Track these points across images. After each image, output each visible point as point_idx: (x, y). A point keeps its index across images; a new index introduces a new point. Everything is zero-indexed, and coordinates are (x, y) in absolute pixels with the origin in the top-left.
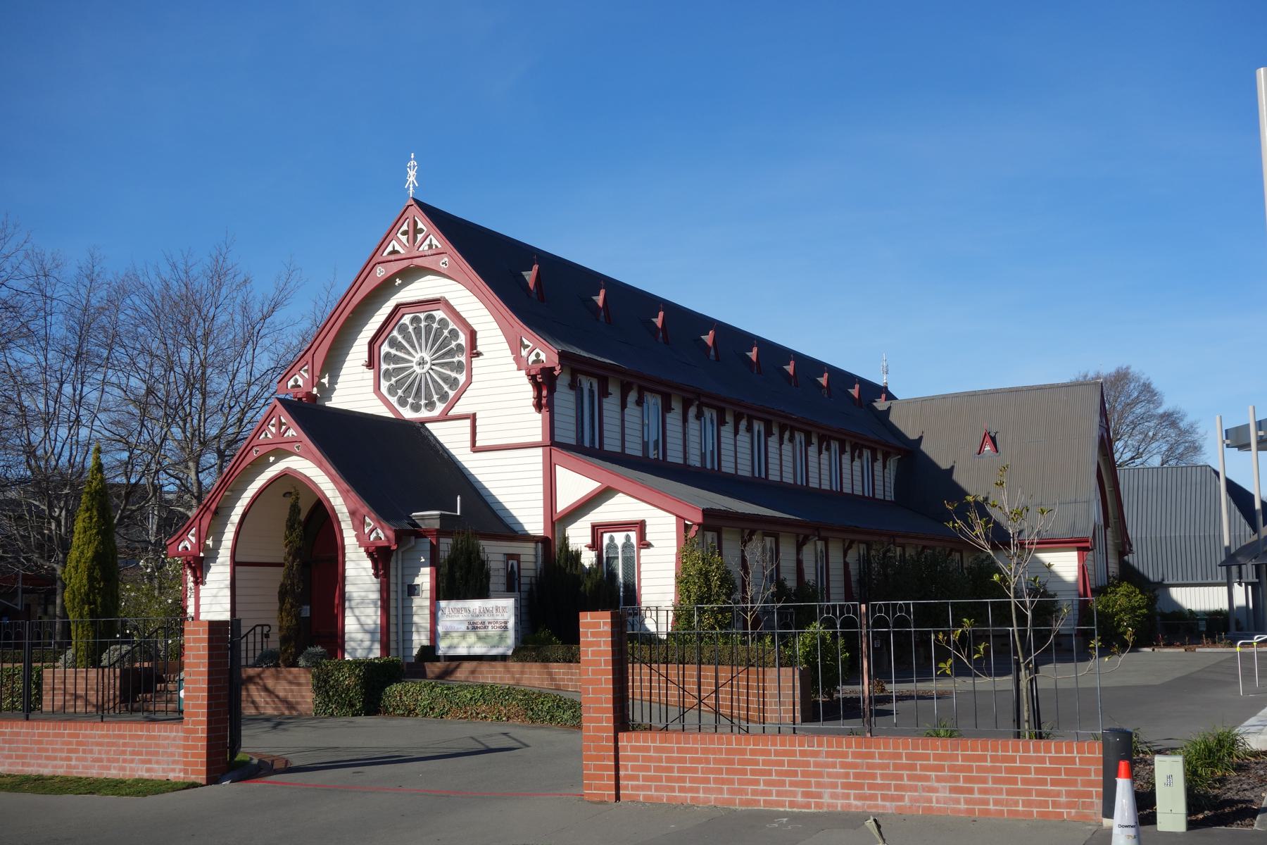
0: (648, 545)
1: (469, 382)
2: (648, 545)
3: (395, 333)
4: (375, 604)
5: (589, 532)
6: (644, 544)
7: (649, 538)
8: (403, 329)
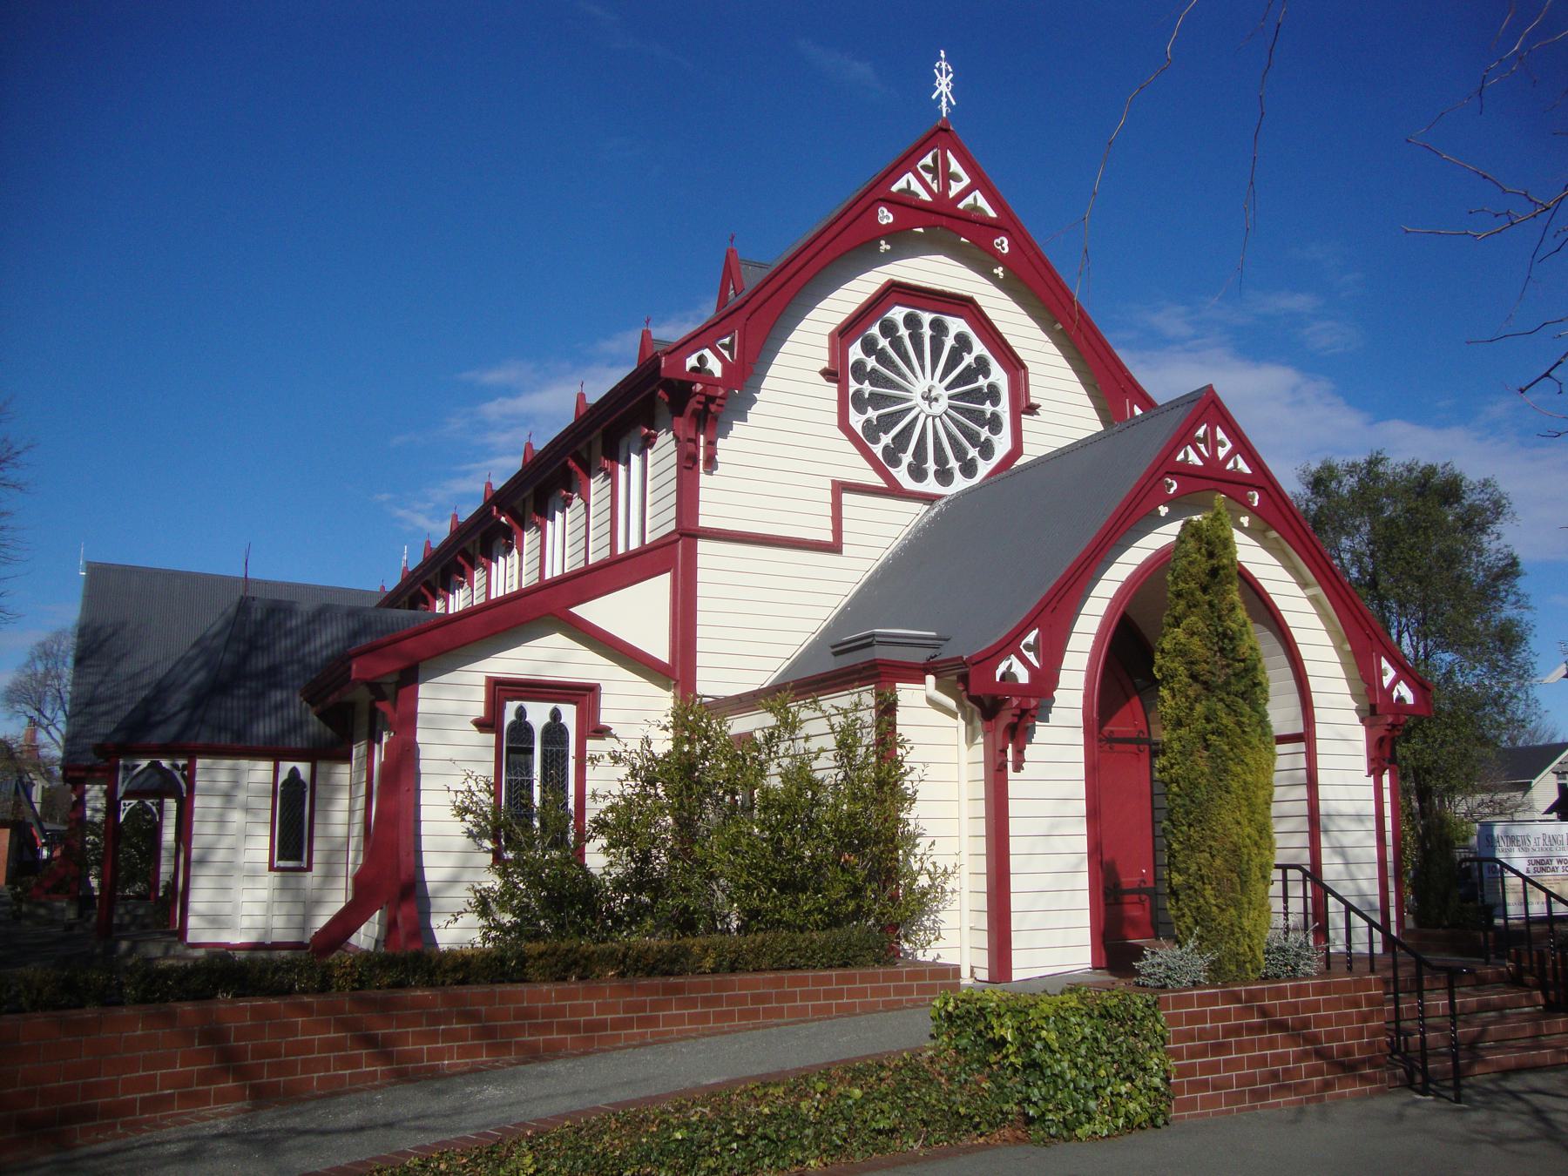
1: (844, 425)
3: (875, 330)
5: (481, 695)
6: (593, 728)
7: (605, 718)
8: (889, 329)
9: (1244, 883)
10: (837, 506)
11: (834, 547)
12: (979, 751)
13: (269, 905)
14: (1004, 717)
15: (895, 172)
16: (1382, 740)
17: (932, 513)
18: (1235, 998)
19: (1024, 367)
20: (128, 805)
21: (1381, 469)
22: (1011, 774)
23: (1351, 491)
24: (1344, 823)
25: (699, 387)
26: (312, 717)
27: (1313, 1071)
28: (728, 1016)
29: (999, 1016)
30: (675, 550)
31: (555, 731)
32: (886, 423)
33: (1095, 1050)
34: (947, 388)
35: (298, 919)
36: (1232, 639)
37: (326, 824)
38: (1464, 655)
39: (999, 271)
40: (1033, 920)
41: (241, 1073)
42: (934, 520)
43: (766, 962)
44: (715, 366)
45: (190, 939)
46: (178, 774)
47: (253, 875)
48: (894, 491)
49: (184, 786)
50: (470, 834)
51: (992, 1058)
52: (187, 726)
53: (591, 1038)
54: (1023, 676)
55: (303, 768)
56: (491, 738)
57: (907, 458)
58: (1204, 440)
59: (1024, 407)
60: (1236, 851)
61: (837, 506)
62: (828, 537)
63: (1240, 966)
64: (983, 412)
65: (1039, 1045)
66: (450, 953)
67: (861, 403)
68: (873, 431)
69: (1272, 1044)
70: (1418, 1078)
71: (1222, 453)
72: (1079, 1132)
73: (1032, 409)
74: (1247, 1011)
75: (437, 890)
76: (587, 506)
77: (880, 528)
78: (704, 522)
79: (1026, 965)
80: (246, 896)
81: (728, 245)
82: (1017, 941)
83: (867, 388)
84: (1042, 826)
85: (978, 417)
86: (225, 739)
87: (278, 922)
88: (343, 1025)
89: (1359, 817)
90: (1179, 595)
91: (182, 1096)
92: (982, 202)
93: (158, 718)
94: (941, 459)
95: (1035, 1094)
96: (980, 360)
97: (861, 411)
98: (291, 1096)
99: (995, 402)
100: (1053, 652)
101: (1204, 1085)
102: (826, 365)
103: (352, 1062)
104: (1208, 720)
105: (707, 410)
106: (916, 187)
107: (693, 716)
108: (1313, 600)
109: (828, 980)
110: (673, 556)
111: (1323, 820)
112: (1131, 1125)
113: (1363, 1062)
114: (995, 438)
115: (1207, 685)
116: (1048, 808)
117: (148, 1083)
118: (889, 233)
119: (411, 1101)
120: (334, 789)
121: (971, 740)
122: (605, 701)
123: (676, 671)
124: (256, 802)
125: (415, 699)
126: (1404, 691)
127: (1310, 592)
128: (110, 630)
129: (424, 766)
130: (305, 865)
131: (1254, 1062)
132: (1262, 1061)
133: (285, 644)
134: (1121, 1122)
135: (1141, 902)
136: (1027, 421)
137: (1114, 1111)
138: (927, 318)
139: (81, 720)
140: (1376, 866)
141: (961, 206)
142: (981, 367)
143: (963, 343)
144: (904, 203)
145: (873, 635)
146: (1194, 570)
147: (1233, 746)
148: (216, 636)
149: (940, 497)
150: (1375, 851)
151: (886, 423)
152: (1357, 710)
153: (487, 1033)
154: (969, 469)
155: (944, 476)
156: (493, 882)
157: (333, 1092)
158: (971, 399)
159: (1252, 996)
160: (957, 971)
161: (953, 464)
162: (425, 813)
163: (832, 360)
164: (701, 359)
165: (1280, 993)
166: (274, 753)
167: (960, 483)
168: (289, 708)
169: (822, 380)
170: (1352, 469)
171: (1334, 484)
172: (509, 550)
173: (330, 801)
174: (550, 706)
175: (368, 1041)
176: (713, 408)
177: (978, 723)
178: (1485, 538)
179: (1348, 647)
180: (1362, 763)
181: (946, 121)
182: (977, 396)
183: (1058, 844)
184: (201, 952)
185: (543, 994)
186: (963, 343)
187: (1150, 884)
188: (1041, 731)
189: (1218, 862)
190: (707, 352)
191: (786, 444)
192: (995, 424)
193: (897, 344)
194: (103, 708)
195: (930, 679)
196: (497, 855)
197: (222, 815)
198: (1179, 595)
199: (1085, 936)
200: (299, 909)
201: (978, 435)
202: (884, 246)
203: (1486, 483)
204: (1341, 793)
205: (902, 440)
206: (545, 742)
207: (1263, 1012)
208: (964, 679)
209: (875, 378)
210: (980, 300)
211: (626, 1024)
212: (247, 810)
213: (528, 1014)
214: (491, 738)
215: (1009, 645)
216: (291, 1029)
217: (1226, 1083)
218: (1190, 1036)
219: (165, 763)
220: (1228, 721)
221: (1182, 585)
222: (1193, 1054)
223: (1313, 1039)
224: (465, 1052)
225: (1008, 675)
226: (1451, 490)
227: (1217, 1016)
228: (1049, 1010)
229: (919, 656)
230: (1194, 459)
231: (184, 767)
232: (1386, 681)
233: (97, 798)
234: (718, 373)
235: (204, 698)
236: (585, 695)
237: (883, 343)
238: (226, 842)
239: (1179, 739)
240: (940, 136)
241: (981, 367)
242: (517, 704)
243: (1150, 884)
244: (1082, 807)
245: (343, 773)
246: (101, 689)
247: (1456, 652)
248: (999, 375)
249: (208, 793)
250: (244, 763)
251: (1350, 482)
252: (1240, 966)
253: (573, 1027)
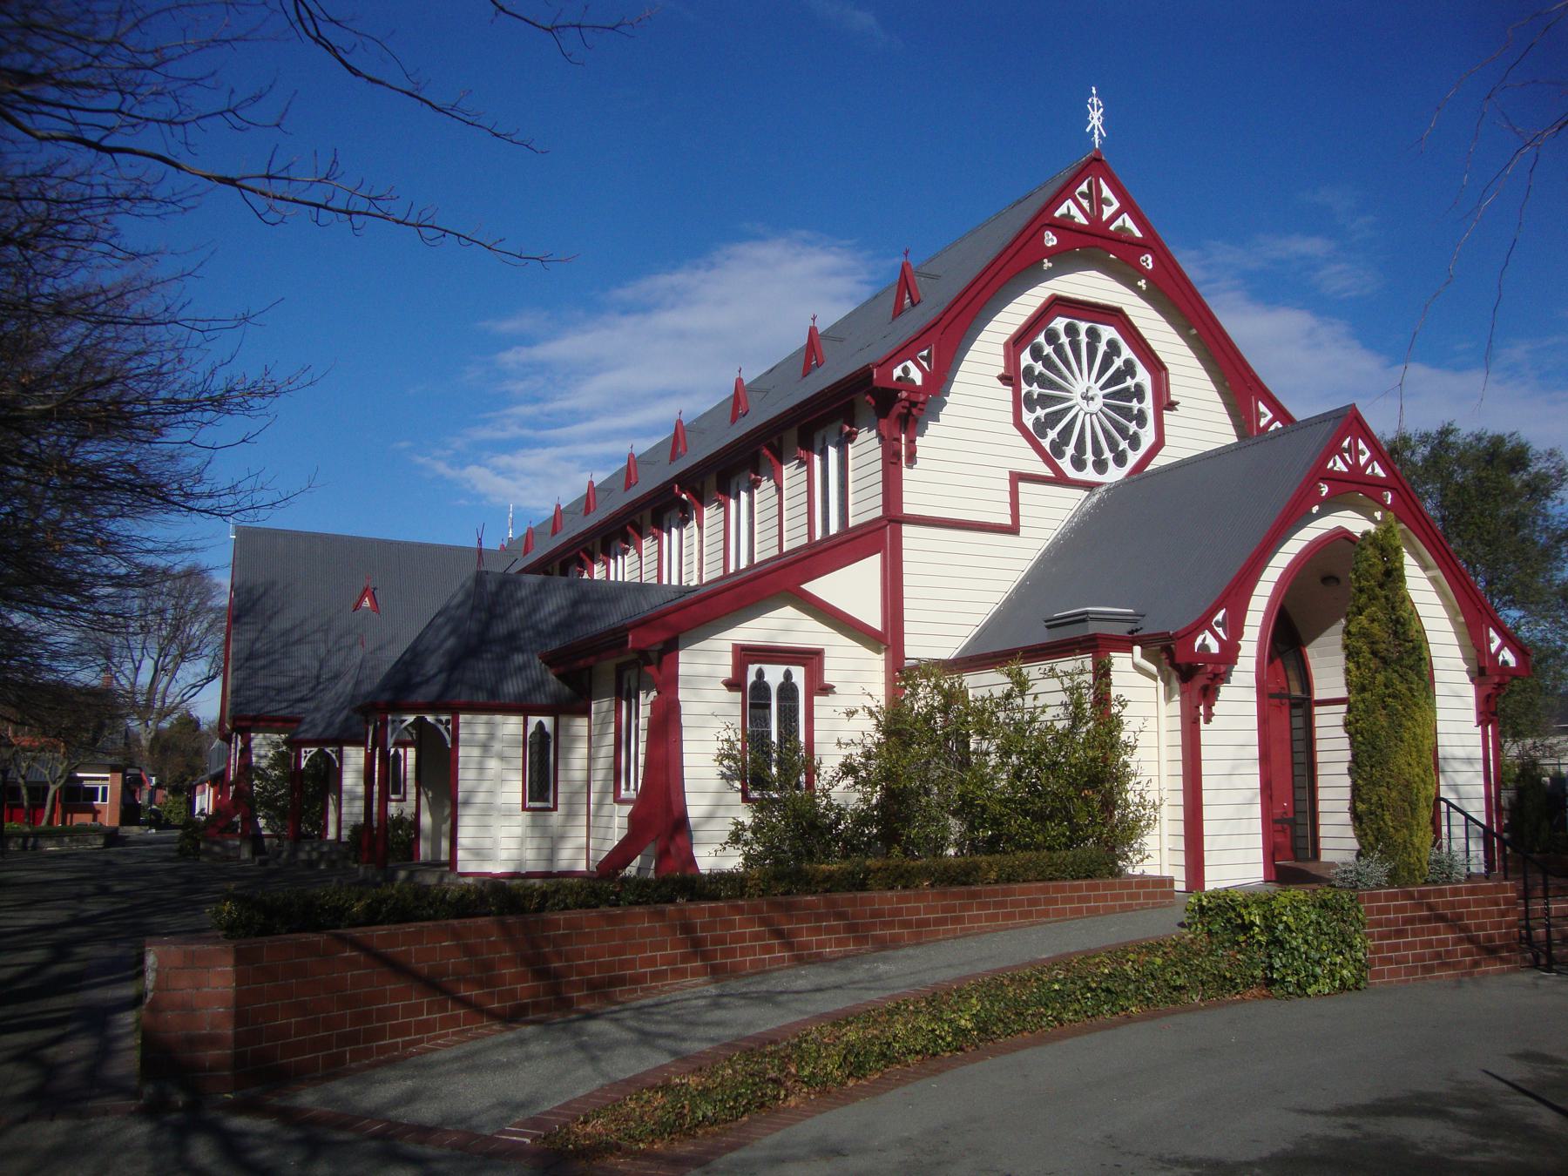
0: (827, 690)
1: (1018, 423)
2: (827, 690)
3: (1041, 339)
4: (357, 771)
5: (728, 659)
6: (819, 687)
7: (828, 678)
8: (1052, 337)
9: (1413, 810)
10: (1014, 494)
11: (1013, 529)
12: (1176, 707)
13: (522, 839)
14: (1196, 680)
15: (1057, 201)
16: (1489, 696)
17: (1095, 499)
18: (1410, 896)
19: (1165, 369)
20: (307, 754)
21: (1451, 438)
22: (1203, 725)
23: (1425, 460)
24: (1457, 765)
25: (904, 394)
26: (552, 677)
27: (1466, 953)
28: (1010, 916)
29: (1246, 907)
30: (884, 534)
31: (787, 690)
32: (1053, 419)
33: (1320, 931)
34: (1102, 389)
35: (545, 852)
36: (1403, 625)
37: (567, 770)
38: (1531, 613)
39: (1142, 283)
40: (1221, 842)
41: (705, 956)
42: (1097, 506)
43: (1031, 875)
44: (916, 376)
45: (460, 869)
46: (442, 728)
47: (508, 814)
48: (1060, 480)
49: (448, 738)
50: (723, 776)
51: (1241, 938)
52: (447, 687)
53: (921, 932)
54: (1215, 648)
55: (548, 722)
56: (739, 695)
57: (1070, 450)
58: (1348, 450)
59: (1165, 403)
60: (1408, 785)
62: (1008, 521)
63: (1411, 873)
64: (1130, 409)
65: (1281, 927)
67: (1031, 403)
68: (1042, 426)
69: (1436, 931)
70: (1543, 961)
71: (1363, 460)
72: (1309, 991)
73: (1172, 406)
74: (1419, 906)
75: (697, 825)
76: (779, 489)
77: (1052, 512)
79: (1217, 877)
80: (503, 832)
81: (903, 259)
82: (1208, 859)
83: (1036, 389)
84: (1225, 767)
85: (1127, 413)
86: (481, 697)
87: (530, 854)
88: (764, 922)
89: (1469, 761)
90: (1361, 590)
91: (673, 971)
92: (1130, 224)
93: (419, 679)
94: (1097, 451)
95: (1277, 963)
96: (1128, 363)
97: (1032, 410)
98: (735, 972)
99: (1141, 400)
100: (1235, 627)
101: (1389, 960)
102: (1002, 371)
103: (768, 949)
104: (1386, 687)
105: (909, 413)
106: (1075, 211)
107: (901, 673)
108: (1433, 580)
109: (1079, 888)
110: (880, 537)
111: (1441, 762)
112: (1344, 987)
113: (1502, 947)
114: (1141, 432)
115: (1384, 661)
116: (1230, 752)
117: (652, 961)
118: (1052, 253)
119: (806, 978)
120: (573, 739)
121: (1168, 698)
122: (828, 663)
123: (886, 638)
124: (508, 752)
125: (675, 663)
126: (1508, 656)
127: (1430, 573)
128: (261, 590)
129: (685, 720)
130: (551, 805)
131: (1424, 944)
132: (1429, 944)
133: (518, 612)
134: (1337, 984)
135: (1283, 830)
136: (1168, 416)
137: (1332, 974)
138: (1083, 326)
139: (242, 674)
140: (1483, 802)
141: (1112, 228)
142: (1129, 369)
143: (1113, 348)
145: (1087, 613)
146: (1373, 571)
147: (1406, 707)
148: (459, 606)
149: (1099, 484)
150: (1482, 789)
151: (1053, 419)
152: (1468, 672)
153: (852, 928)
154: (1120, 459)
155: (1101, 466)
156: (747, 818)
157: (761, 971)
158: (1121, 398)
159: (1423, 895)
160: (1171, 881)
161: (1108, 455)
162: (687, 760)
163: (1007, 367)
164: (906, 370)
165: (1441, 893)
166: (522, 708)
167: (1115, 474)
168: (530, 670)
169: (999, 384)
170: (1425, 438)
171: (1407, 454)
172: (684, 522)
173: (569, 749)
174: (784, 668)
175: (779, 934)
176: (914, 411)
177: (1176, 685)
178: (1549, 504)
179: (1462, 619)
180: (1472, 715)
181: (1098, 152)
182: (1126, 395)
183: (1237, 781)
184: (470, 880)
185: (885, 899)
186: (1113, 348)
187: (1291, 816)
188: (1224, 691)
189: (1394, 794)
190: (909, 364)
191: (972, 442)
192: (1141, 419)
193: (1059, 350)
194: (262, 662)
195: (1137, 649)
196: (744, 792)
197: (481, 763)
198: (1361, 590)
199: (1259, 855)
200: (546, 844)
201: (1127, 429)
202: (1047, 264)
203: (1551, 454)
204: (1455, 740)
205: (1065, 434)
206: (780, 699)
207: (1430, 907)
208: (1167, 650)
209: (1042, 381)
210: (1127, 310)
211: (938, 922)
212: (502, 758)
213: (876, 914)
214: (739, 695)
215: (1204, 623)
216: (731, 924)
217: (1404, 959)
218: (1379, 924)
219: (430, 718)
220: (1402, 687)
221: (1364, 583)
222: (1382, 936)
223: (1465, 929)
224: (839, 943)
225: (1204, 646)
226: (1518, 458)
227: (1398, 909)
228: (1287, 902)
229: (1121, 630)
230: (1340, 466)
231: (448, 722)
232: (1494, 647)
233: (261, 745)
234: (919, 382)
235: (456, 663)
236: (811, 659)
237: (1048, 350)
238: (485, 786)
239: (1363, 701)
240: (1095, 166)
241: (1129, 369)
242: (757, 666)
243: (1291, 816)
244: (1255, 752)
245: (581, 725)
246: (258, 645)
247: (1522, 607)
248: (1143, 376)
249: (470, 744)
250: (498, 718)
251: (1424, 450)
252: (1411, 873)
253: (906, 924)
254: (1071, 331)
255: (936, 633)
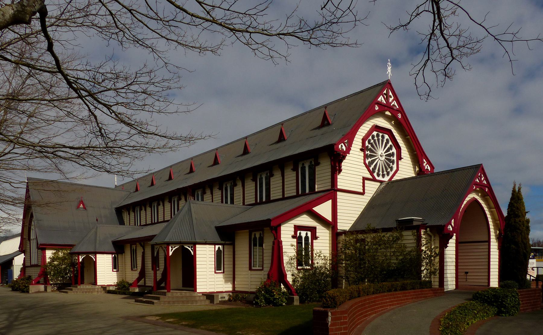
1: (365, 163)
3: (370, 138)
6: (314, 237)
7: (318, 235)
10: (364, 183)
11: (363, 194)
34: (386, 156)
46: (174, 249)
48: (374, 180)
49: (192, 253)
61: (364, 183)
66: (528, 262)
77: (372, 188)
78: (339, 187)
92: (396, 104)
102: (361, 147)
106: (383, 99)
107: (336, 235)
123: (331, 225)
136: (400, 162)
144: (380, 104)
155: (383, 176)
161: (381, 173)
174: (305, 232)
209: (371, 151)
236: (313, 230)
254: (378, 135)
255: (345, 223)
